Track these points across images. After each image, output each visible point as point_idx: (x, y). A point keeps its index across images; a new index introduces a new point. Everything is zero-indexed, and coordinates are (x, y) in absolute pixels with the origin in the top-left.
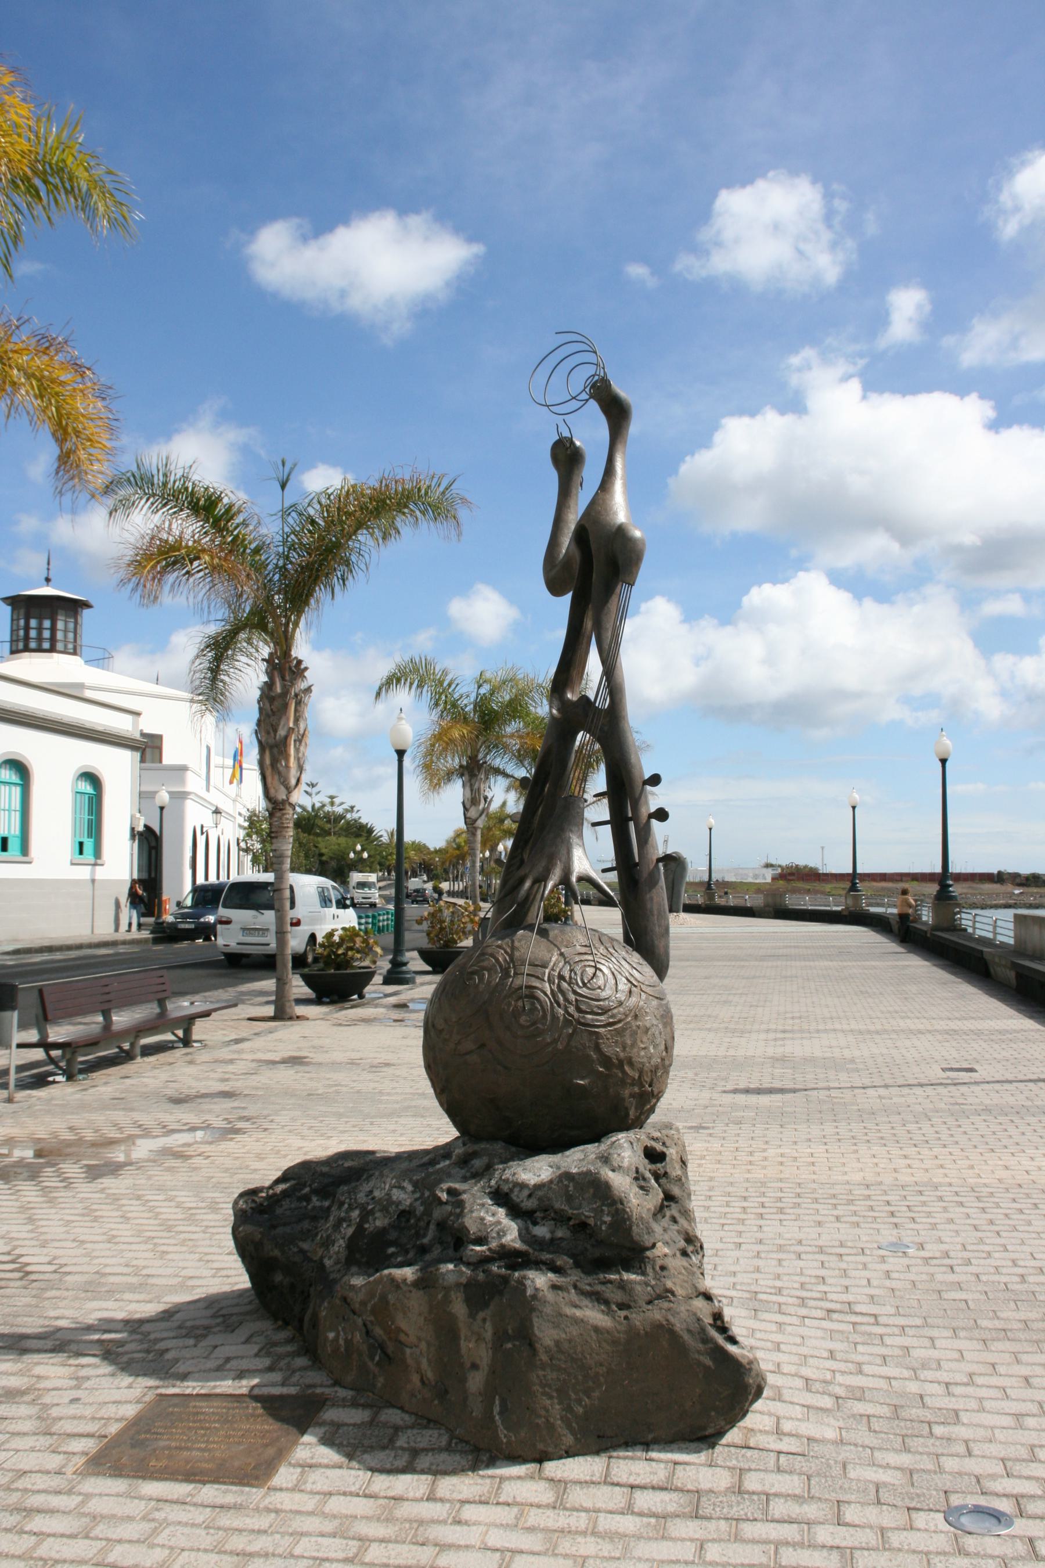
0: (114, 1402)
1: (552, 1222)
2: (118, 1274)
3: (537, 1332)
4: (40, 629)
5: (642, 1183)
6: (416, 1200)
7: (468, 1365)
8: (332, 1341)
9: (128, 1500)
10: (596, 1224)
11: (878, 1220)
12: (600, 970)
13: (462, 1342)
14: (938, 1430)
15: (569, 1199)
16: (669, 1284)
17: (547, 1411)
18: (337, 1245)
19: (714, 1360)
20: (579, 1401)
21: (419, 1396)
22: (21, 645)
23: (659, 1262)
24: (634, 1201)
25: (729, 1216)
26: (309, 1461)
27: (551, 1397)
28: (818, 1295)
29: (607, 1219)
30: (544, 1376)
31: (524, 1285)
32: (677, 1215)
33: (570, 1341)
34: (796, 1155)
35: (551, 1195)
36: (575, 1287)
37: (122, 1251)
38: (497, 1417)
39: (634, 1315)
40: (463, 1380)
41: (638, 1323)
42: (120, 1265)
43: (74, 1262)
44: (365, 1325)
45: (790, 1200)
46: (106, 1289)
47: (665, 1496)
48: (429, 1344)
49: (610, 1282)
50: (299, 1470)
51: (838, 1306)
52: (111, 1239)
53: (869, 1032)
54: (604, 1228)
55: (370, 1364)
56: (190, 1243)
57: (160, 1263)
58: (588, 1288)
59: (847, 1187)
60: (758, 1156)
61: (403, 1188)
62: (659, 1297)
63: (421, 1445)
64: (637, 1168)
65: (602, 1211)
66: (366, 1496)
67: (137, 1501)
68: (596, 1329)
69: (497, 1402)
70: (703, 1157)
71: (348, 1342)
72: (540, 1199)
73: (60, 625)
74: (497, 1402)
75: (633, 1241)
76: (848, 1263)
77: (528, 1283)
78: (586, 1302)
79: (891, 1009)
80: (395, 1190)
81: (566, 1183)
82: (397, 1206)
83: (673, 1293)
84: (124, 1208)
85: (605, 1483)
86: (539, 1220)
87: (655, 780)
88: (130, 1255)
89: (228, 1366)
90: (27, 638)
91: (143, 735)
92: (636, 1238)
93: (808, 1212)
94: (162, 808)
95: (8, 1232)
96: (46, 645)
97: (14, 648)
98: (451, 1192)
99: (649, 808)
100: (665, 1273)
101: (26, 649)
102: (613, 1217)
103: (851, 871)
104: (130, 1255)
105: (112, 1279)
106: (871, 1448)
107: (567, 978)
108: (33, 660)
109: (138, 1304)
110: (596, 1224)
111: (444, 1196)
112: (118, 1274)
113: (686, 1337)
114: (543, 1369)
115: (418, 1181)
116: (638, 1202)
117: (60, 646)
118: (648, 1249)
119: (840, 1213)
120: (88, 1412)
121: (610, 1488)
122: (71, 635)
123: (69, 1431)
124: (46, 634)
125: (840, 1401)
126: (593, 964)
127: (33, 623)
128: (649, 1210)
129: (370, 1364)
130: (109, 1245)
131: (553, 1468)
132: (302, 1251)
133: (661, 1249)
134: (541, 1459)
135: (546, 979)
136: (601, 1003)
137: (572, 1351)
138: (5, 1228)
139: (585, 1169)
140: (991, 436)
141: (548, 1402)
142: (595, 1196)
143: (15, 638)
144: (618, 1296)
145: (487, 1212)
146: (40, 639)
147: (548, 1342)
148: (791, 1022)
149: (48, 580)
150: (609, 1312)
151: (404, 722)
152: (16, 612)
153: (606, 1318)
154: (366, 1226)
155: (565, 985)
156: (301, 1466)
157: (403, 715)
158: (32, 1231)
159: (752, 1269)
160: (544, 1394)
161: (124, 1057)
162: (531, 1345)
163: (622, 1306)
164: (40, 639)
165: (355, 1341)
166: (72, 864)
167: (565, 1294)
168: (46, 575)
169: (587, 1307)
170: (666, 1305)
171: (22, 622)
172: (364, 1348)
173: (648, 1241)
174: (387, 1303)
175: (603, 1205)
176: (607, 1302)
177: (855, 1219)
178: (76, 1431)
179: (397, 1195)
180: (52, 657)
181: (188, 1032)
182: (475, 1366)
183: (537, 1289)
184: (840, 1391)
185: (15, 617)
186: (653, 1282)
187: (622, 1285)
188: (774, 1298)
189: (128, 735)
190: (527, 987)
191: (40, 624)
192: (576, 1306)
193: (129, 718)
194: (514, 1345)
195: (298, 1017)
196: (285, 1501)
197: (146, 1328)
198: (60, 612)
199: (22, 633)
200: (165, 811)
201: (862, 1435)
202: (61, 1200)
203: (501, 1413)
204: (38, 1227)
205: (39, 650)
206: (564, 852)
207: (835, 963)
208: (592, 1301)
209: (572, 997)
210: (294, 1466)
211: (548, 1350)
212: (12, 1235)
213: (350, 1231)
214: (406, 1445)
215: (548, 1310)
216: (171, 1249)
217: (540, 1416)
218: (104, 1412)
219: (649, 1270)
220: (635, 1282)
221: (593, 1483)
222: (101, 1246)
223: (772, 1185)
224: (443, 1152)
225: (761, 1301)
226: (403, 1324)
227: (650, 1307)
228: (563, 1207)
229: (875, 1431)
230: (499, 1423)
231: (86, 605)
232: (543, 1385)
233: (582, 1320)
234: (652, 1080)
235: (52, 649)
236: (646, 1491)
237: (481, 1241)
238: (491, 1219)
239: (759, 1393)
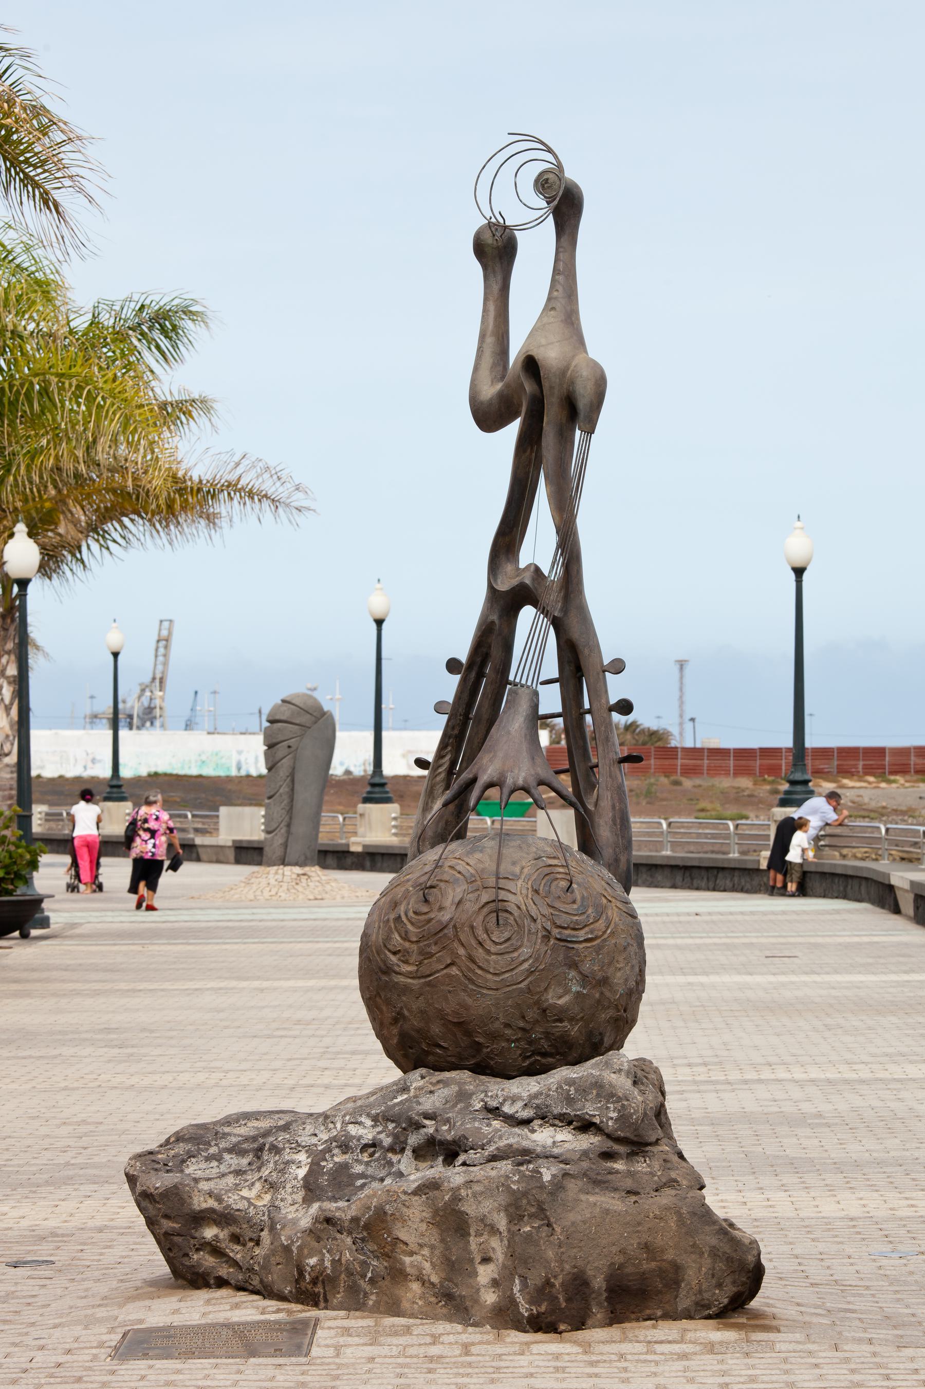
10: (602, 1122)
15: (570, 1100)
29: (614, 1115)
33: (584, 1222)
35: (549, 1102)
38: (518, 1295)
53: (846, 1081)
54: (610, 1123)
55: (362, 1282)
61: (360, 1123)
65: (608, 1108)
69: (517, 1281)
71: (336, 1263)
74: (517, 1281)
79: (890, 1050)
80: (350, 1127)
82: (359, 1140)
86: (536, 1128)
87: (618, 667)
99: (608, 701)
102: (619, 1111)
103: (786, 741)
110: (602, 1122)
118: (650, 1144)
128: (651, 1108)
142: (598, 1095)
144: (629, 1183)
148: (687, 1070)
150: (622, 1199)
175: (608, 1102)
197: (633, 949)
207: (758, 979)
228: (564, 1111)
234: (627, 1004)
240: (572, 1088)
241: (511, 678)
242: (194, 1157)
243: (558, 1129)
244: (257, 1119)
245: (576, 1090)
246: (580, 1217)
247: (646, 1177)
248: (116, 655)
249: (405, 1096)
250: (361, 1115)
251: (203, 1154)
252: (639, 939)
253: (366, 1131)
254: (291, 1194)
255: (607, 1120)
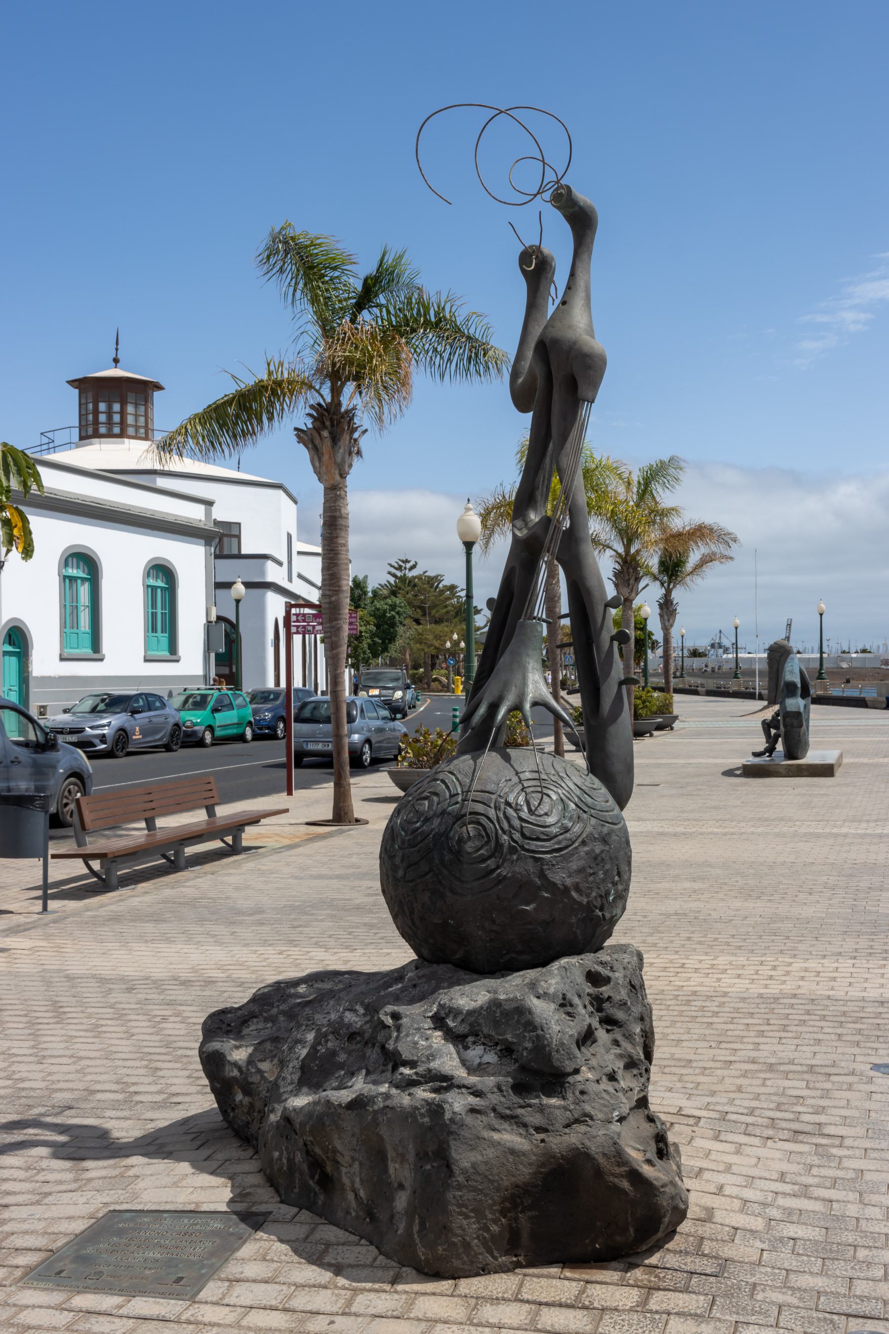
0: (67, 1218)
1: (482, 1047)
2: (107, 1091)
3: (454, 1154)
4: (109, 414)
5: (569, 1009)
6: (366, 1022)
7: (396, 1185)
8: (277, 1160)
9: (58, 1312)
11: (881, 1039)
12: (548, 796)
13: (389, 1162)
14: (862, 1254)
15: (496, 1024)
16: (588, 1108)
17: (464, 1230)
18: (291, 1065)
19: (632, 1184)
20: (495, 1221)
21: (354, 1214)
22: (90, 431)
23: (580, 1087)
24: (556, 1028)
25: (729, 1033)
26: (237, 1276)
27: (467, 1217)
28: (791, 1116)
29: (529, 1045)
30: (461, 1196)
31: (443, 1108)
32: (620, 1038)
33: (486, 1163)
34: (821, 969)
36: (494, 1110)
37: (117, 1067)
38: (416, 1236)
39: (551, 1138)
40: (391, 1199)
41: (554, 1147)
42: (111, 1082)
43: (66, 1078)
44: (305, 1145)
45: (797, 1017)
46: (92, 1105)
47: (570, 1313)
48: (361, 1164)
49: (530, 1106)
50: (227, 1284)
51: (808, 1128)
52: (108, 1056)
55: (311, 1182)
56: (185, 1060)
57: (151, 1079)
58: (508, 1112)
59: (861, 1004)
60: (779, 972)
62: (577, 1121)
63: (346, 1261)
64: (564, 994)
65: (524, 1037)
66: (285, 1310)
67: (66, 1313)
68: (512, 1151)
69: (417, 1221)
70: (724, 971)
71: (290, 1161)
72: (471, 1025)
73: (130, 409)
74: (417, 1221)
75: (553, 1066)
76: (833, 1083)
77: (447, 1106)
78: (506, 1125)
80: (347, 1014)
81: (494, 1009)
82: (348, 1028)
83: (591, 1118)
84: (130, 1024)
85: (517, 1300)
88: (125, 1071)
89: (184, 1183)
90: (96, 422)
91: (217, 523)
92: (556, 1064)
93: (811, 1029)
94: (238, 601)
95: (9, 1048)
96: (117, 430)
97: (83, 434)
98: (396, 1016)
100: (585, 1097)
101: (97, 435)
104: (125, 1071)
105: (99, 1096)
106: (787, 1270)
107: (513, 805)
108: (104, 446)
109: (118, 1122)
111: (389, 1021)
112: (107, 1091)
113: (601, 1160)
114: (460, 1189)
115: (369, 1004)
116: (558, 1028)
117: (131, 431)
118: (569, 1074)
119: (844, 1031)
120: (40, 1226)
121: (519, 1304)
122: (142, 420)
123: (18, 1246)
124: (117, 418)
125: (773, 1223)
126: (539, 789)
127: (102, 407)
128: (571, 1036)
129: (311, 1182)
130: (106, 1061)
131: (468, 1285)
132: (259, 1071)
133: (587, 1074)
134: (455, 1276)
135: (492, 805)
136: (547, 829)
137: (488, 1173)
138: (7, 1044)
139: (512, 996)
140: (30, 561)
141: (465, 1222)
143: (83, 423)
144: (535, 1119)
145: (421, 1037)
146: (110, 423)
147: (466, 1164)
149: (116, 361)
150: (528, 1136)
151: (471, 513)
152: (84, 395)
153: (524, 1141)
154: (319, 1048)
155: (510, 812)
156: (229, 1280)
157: (470, 505)
158: (33, 1047)
159: (733, 1088)
160: (460, 1214)
161: (173, 866)
162: (448, 1166)
163: (539, 1129)
164: (110, 423)
165: (297, 1160)
166: (146, 660)
167: (484, 1118)
168: (114, 356)
169: (505, 1130)
170: (582, 1128)
171: (90, 406)
172: (305, 1167)
173: (569, 1067)
174: (324, 1124)
175: (525, 1031)
176: (525, 1125)
177: (857, 1038)
178: (25, 1245)
179: (349, 1017)
180: (123, 443)
181: (237, 839)
182: (401, 1186)
183: (454, 1113)
184: (775, 1213)
185: (83, 401)
186: (572, 1107)
187: (541, 1109)
188: (743, 1118)
189: (202, 525)
190: (471, 813)
191: (110, 407)
192: (494, 1130)
193: (202, 508)
194: (433, 1167)
195: (357, 821)
196: (209, 1314)
198: (129, 394)
199: (90, 417)
200: (241, 604)
201: (786, 1258)
202: (69, 1015)
203: (419, 1232)
204: (39, 1043)
205: (110, 435)
206: (518, 677)
208: (511, 1124)
209: (516, 823)
210: (222, 1280)
211: (464, 1171)
212: (13, 1051)
213: (304, 1052)
214: (333, 1262)
215: (465, 1133)
216: (164, 1065)
217: (456, 1235)
218: (55, 1229)
219: (570, 1095)
220: (554, 1107)
221: (504, 1299)
222: (98, 1062)
223: (785, 1001)
224: (398, 975)
225: (729, 1121)
226: (338, 1144)
227: (567, 1130)
229: (798, 1254)
230: (417, 1241)
231: (158, 387)
232: (460, 1206)
233: (499, 1143)
235: (122, 435)
236: (553, 1309)
237: (412, 1064)
238: (424, 1043)
239: (681, 1215)
240: (498, 1011)
241: (535, 614)
242: (256, 1017)
243: (488, 1048)
244: (322, 981)
245: (502, 1013)
246: (480, 1158)
247: (558, 1112)
248: (736, 628)
249: (400, 986)
250: (356, 1003)
251: (265, 1014)
252: (628, 842)
253: (357, 1019)
254: (291, 1074)
255: (523, 1050)
